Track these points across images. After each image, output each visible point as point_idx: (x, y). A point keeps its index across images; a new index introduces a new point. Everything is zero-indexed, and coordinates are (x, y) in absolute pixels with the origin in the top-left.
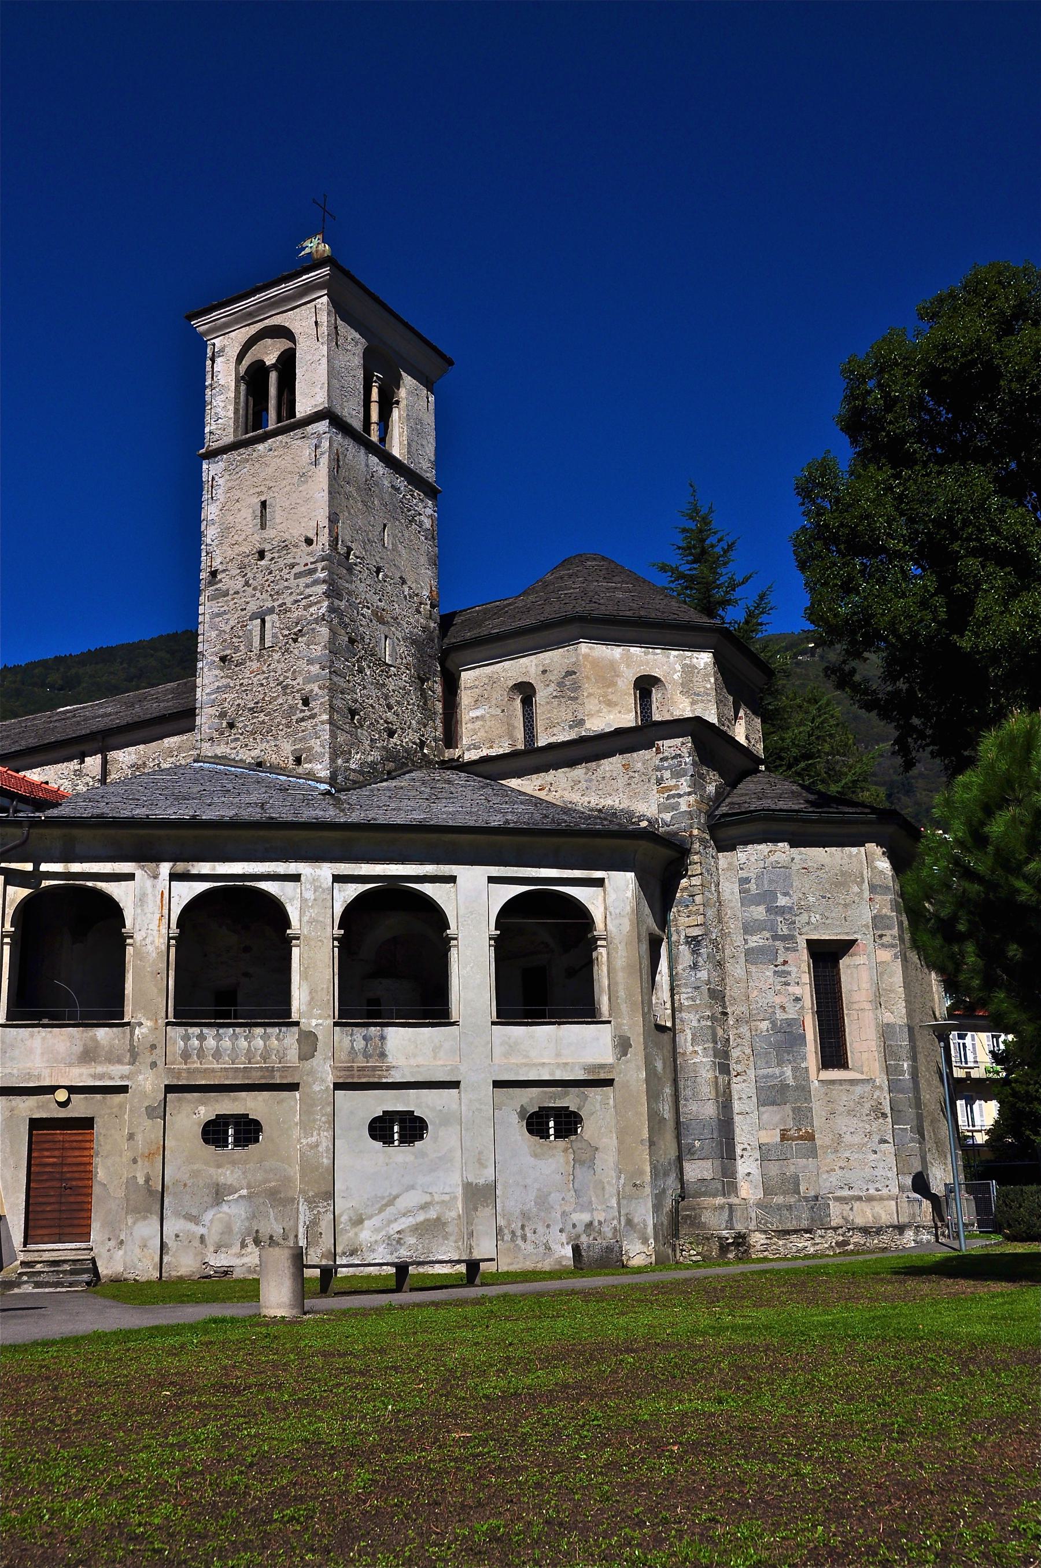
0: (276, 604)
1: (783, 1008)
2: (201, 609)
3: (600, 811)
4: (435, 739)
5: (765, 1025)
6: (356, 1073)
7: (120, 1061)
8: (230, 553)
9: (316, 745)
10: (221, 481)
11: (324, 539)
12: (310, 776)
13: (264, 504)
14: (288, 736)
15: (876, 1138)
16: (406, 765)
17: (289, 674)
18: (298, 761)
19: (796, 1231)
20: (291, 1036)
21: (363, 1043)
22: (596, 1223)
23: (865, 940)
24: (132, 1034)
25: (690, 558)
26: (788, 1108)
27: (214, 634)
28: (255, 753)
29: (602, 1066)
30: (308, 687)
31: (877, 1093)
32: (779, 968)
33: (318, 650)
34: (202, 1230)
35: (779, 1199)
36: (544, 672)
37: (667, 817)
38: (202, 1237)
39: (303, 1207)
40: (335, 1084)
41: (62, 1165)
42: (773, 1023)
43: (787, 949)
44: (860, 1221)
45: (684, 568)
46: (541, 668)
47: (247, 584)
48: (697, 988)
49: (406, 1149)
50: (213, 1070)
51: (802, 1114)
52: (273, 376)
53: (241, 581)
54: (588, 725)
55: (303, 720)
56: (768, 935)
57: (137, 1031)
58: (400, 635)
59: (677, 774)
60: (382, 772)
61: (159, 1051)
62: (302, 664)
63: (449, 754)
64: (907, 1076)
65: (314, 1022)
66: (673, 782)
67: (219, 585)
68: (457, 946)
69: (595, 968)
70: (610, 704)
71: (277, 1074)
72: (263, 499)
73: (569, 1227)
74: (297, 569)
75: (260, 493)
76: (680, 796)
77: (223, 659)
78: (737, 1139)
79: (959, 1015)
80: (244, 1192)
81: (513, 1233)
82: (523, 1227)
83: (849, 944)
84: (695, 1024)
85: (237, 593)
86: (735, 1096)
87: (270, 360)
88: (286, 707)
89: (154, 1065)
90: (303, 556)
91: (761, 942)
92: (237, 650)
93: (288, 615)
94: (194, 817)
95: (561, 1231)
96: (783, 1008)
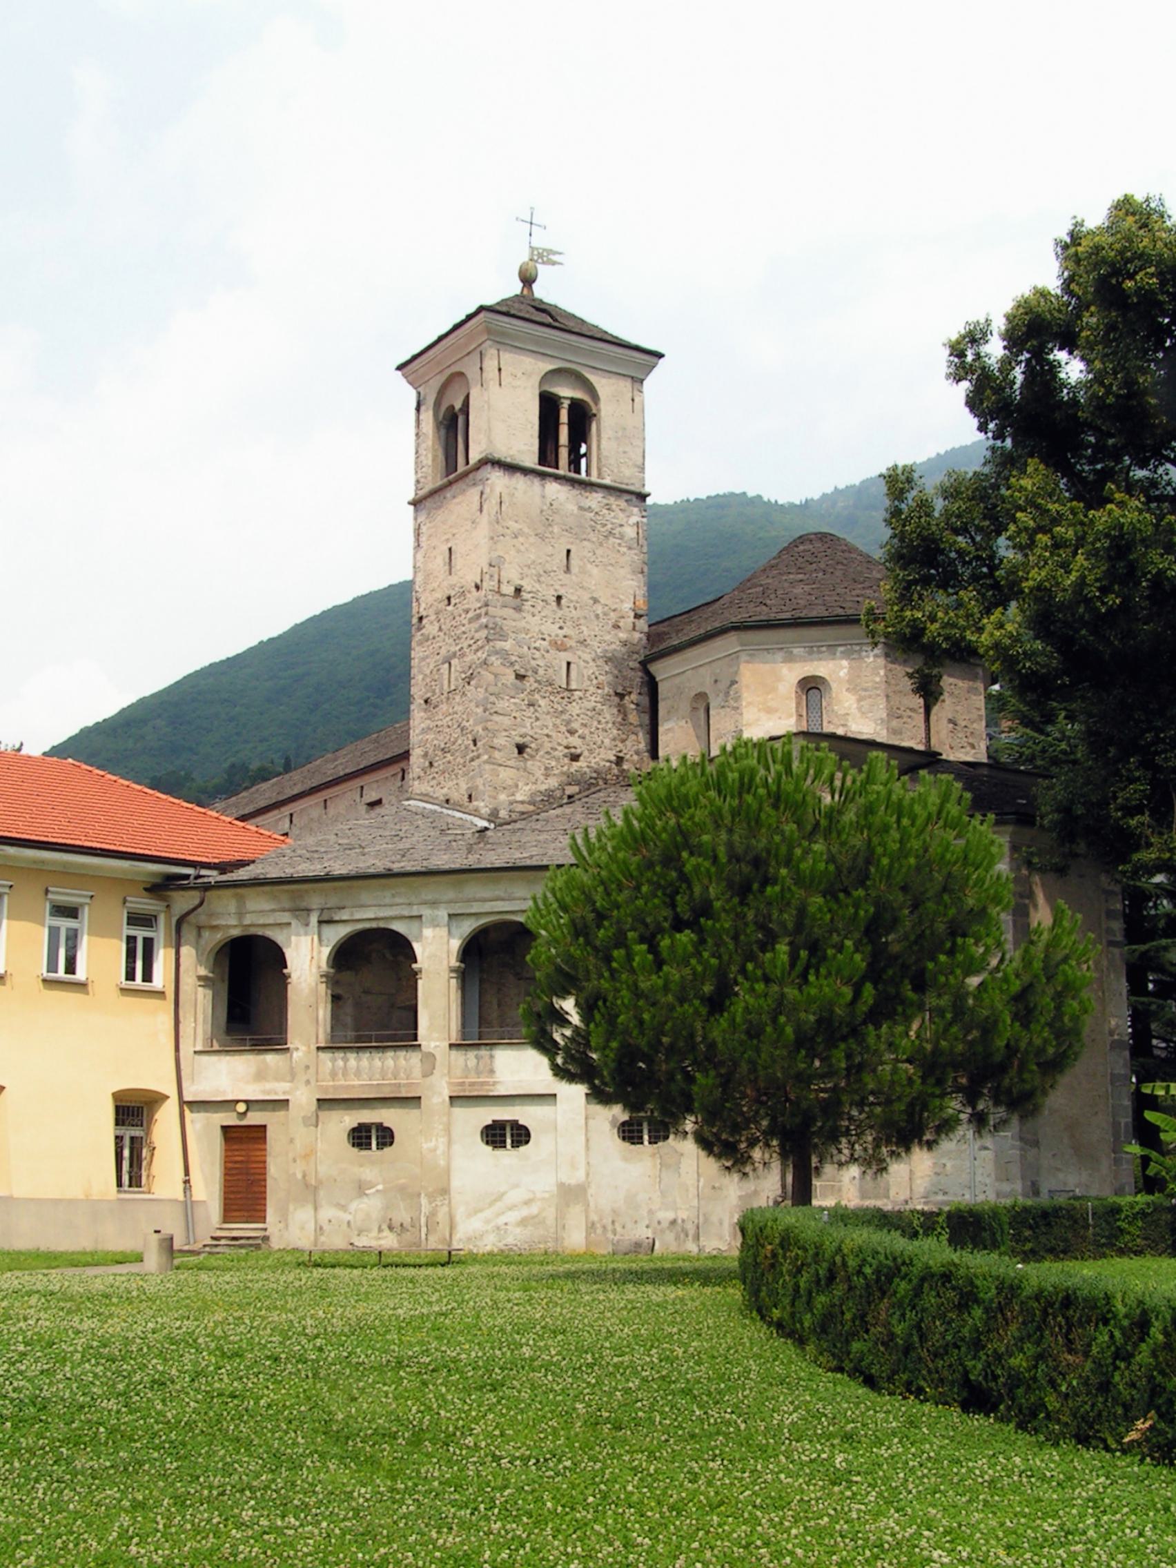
4: (637, 753)
6: (467, 1087)
7: (283, 1080)
16: (597, 784)
20: (414, 1058)
21: (475, 1061)
22: (679, 1221)
27: (420, 677)
34: (350, 1217)
39: (424, 1201)
40: (451, 1097)
41: (247, 1162)
47: (440, 629)
50: (353, 1086)
57: (295, 1055)
58: (588, 657)
60: (561, 798)
61: (312, 1070)
65: (433, 1044)
70: (769, 711)
80: (380, 1187)
81: (604, 1227)
95: (647, 1227)
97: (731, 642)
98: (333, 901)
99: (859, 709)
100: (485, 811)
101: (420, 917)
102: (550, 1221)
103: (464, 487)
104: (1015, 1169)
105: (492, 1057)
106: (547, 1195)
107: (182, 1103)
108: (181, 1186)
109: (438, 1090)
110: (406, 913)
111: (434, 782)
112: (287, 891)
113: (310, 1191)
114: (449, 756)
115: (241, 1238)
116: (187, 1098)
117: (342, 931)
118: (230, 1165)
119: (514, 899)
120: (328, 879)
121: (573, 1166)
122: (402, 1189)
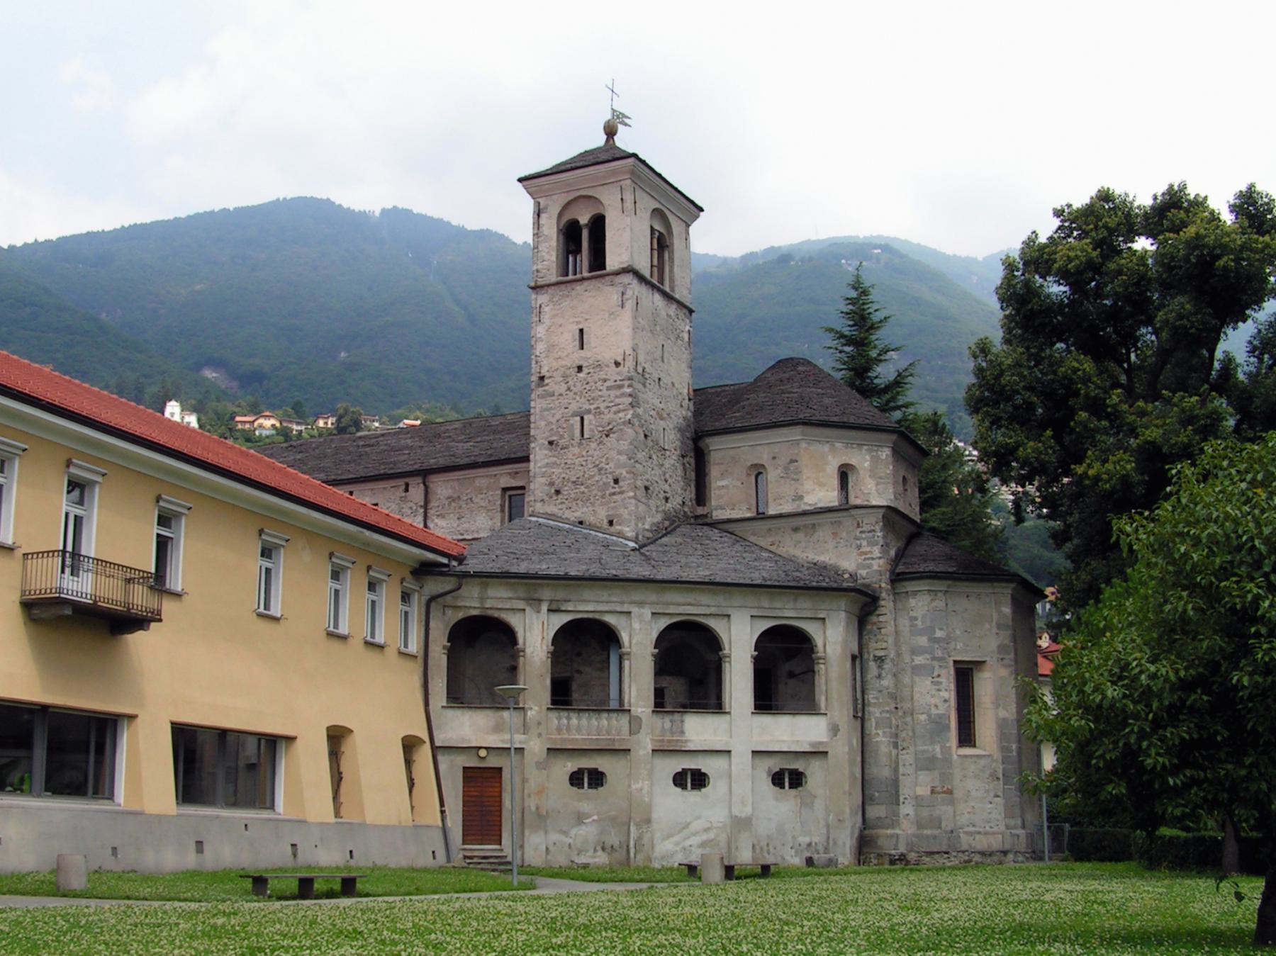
0: (592, 407)
1: (936, 706)
2: (532, 404)
3: (815, 564)
5: (923, 717)
8: (555, 365)
9: (624, 513)
10: (547, 309)
11: (630, 363)
12: (620, 535)
13: (581, 331)
14: (602, 504)
15: (992, 794)
17: (603, 460)
18: (611, 523)
19: (938, 853)
20: (624, 720)
23: (991, 660)
24: (525, 715)
25: (851, 323)
26: (936, 773)
27: (543, 423)
28: (578, 514)
29: (821, 743)
30: (618, 471)
31: (994, 764)
32: (936, 679)
33: (624, 445)
34: (571, 841)
35: (927, 832)
36: (774, 458)
37: (863, 572)
38: (570, 845)
39: (633, 828)
42: (929, 716)
43: (940, 666)
44: (979, 847)
45: (846, 331)
46: (772, 455)
47: (569, 389)
48: (880, 691)
49: (695, 792)
50: (577, 739)
51: (946, 777)
52: (585, 234)
53: (564, 387)
54: (806, 500)
55: (614, 494)
56: (928, 657)
57: (529, 713)
59: (871, 544)
62: (613, 453)
63: (700, 511)
64: (1014, 753)
65: (640, 710)
66: (868, 549)
67: (546, 388)
68: (730, 662)
69: (817, 677)
70: (821, 485)
71: (617, 743)
72: (581, 327)
73: (797, 846)
74: (609, 383)
75: (578, 323)
76: (873, 559)
77: (551, 443)
78: (901, 792)
79: (876, 248)
80: (595, 817)
81: (761, 849)
82: (768, 845)
83: (980, 664)
84: (878, 715)
85: (561, 395)
86: (901, 763)
87: (584, 220)
88: (601, 483)
89: (540, 735)
90: (613, 374)
91: (924, 662)
92: (562, 437)
93: (602, 416)
94: (566, 574)
96: (936, 706)
97: (795, 433)
98: (561, 594)
99: (877, 490)
100: (631, 534)
101: (630, 613)
102: (723, 844)
103: (600, 285)
104: (1017, 811)
105: (682, 721)
106: (720, 825)
107: (435, 749)
108: (439, 814)
109: (644, 743)
110: (619, 609)
111: (564, 506)
112: (526, 584)
113: (542, 819)
114: (582, 488)
115: (491, 857)
116: (438, 744)
117: (566, 618)
118: (466, 799)
119: (701, 605)
120: (566, 577)
121: (743, 803)
122: (613, 820)
